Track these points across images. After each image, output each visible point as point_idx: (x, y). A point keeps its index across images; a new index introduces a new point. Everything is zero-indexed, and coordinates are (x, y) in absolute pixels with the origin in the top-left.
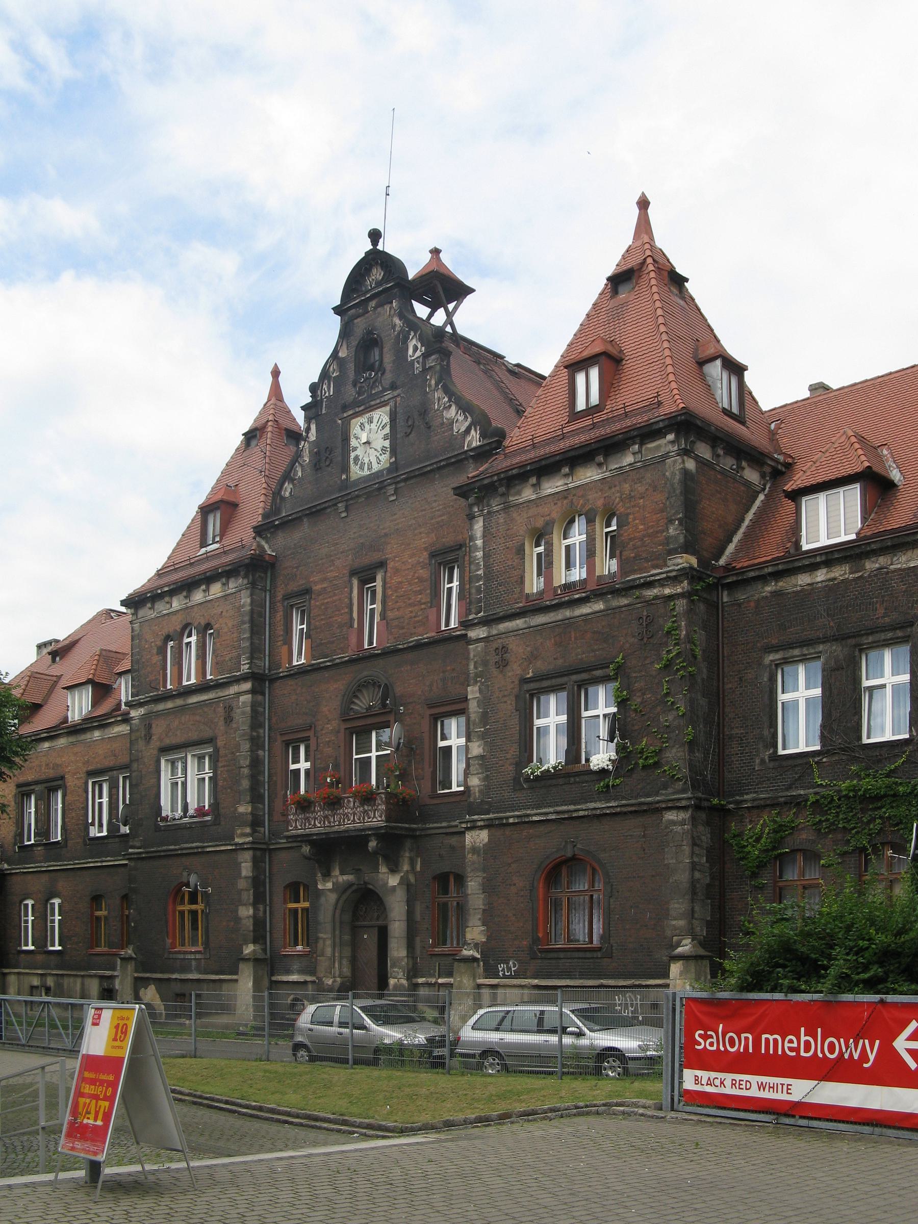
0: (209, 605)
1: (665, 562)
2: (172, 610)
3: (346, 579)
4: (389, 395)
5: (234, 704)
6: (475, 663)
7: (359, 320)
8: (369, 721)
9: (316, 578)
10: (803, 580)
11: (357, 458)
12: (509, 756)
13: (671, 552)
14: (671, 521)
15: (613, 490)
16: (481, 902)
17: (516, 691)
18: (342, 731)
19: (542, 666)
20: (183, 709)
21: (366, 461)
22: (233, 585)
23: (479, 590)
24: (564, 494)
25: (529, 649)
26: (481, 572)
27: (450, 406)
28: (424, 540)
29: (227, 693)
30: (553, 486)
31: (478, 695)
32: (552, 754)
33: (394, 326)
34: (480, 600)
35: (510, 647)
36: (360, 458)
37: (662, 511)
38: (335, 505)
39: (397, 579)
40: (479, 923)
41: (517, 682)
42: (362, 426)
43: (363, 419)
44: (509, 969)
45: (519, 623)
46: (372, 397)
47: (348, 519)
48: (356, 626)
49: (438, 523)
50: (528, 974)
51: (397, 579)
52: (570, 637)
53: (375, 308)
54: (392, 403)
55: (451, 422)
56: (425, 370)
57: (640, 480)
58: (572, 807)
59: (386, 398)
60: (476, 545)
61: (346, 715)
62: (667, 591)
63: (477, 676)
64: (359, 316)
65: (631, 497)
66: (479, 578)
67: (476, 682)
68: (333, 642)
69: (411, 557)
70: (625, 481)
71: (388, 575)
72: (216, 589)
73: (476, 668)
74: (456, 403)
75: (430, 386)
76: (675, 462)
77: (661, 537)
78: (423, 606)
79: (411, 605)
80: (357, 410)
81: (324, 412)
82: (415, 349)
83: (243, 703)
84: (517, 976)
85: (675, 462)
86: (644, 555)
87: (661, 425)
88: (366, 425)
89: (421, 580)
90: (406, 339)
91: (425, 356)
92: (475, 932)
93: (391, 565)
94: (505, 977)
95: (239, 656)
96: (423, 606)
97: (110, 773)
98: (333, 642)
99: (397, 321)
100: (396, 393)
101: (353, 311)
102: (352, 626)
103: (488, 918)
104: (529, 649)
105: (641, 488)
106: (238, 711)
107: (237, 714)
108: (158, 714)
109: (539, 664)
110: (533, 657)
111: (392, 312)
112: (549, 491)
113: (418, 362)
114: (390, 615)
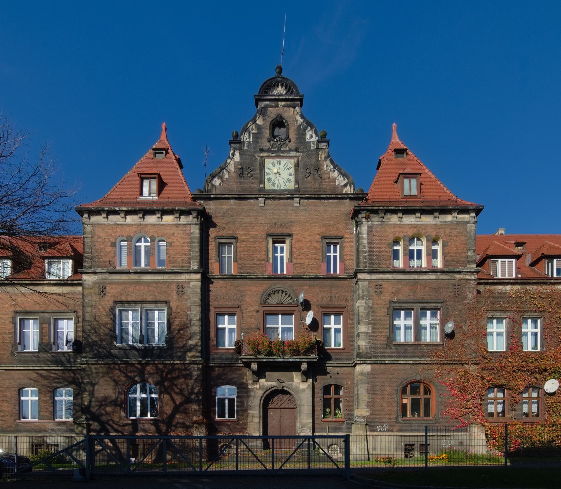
0: (162, 227)
1: (466, 265)
2: (125, 223)
3: (264, 237)
4: (293, 154)
5: (186, 285)
6: (363, 290)
7: (271, 109)
8: (279, 309)
9: (241, 233)
10: (500, 287)
11: (269, 180)
12: (382, 334)
13: (469, 262)
14: (469, 250)
15: (441, 230)
16: (367, 398)
17: (388, 306)
18: (262, 311)
19: (401, 297)
20: (138, 282)
21: (277, 182)
22: (184, 220)
23: (365, 257)
24: (415, 226)
25: (394, 289)
26: (366, 250)
27: (334, 171)
28: (317, 230)
29: (179, 278)
30: (409, 220)
31: (364, 305)
32: (401, 337)
33: (297, 121)
34: (366, 262)
35: (384, 286)
36: (273, 180)
37: (465, 244)
38: (257, 198)
39: (298, 245)
40: (366, 407)
41: (388, 302)
42: (273, 164)
43: (275, 161)
44: (383, 428)
45: (389, 276)
46: (279, 151)
47: (264, 208)
48: (271, 261)
49: (327, 224)
50: (394, 430)
51: (298, 245)
52: (417, 288)
53: (284, 106)
54: (296, 159)
55: (335, 179)
56: (318, 149)
57: (455, 229)
58: (419, 359)
59: (291, 155)
60: (362, 237)
61: (264, 304)
62: (467, 277)
63: (363, 296)
64: (272, 107)
65: (449, 235)
66: (365, 252)
67: (363, 299)
68: (254, 267)
69: (310, 235)
70: (447, 227)
71: (294, 241)
72: (168, 219)
73: (363, 292)
74: (338, 170)
75: (321, 158)
76: (472, 226)
77: (464, 255)
78: (317, 261)
79: (309, 258)
80: (271, 154)
81: (245, 148)
82: (312, 137)
83: (193, 286)
84: (388, 431)
85: (472, 226)
86: (456, 260)
87: (471, 208)
88: (276, 164)
89: (315, 248)
90: (305, 129)
91: (319, 142)
92: (362, 411)
93: (295, 237)
94: (380, 431)
95: (189, 260)
96: (317, 261)
97: (42, 314)
98: (254, 267)
99: (299, 118)
100: (298, 154)
101: (268, 103)
102: (268, 261)
103: (370, 405)
104: (394, 289)
105: (455, 233)
106: (189, 289)
107: (188, 291)
108: (112, 282)
109: (400, 296)
110: (397, 292)
111: (296, 113)
112: (406, 222)
113: (313, 144)
114: (295, 261)
